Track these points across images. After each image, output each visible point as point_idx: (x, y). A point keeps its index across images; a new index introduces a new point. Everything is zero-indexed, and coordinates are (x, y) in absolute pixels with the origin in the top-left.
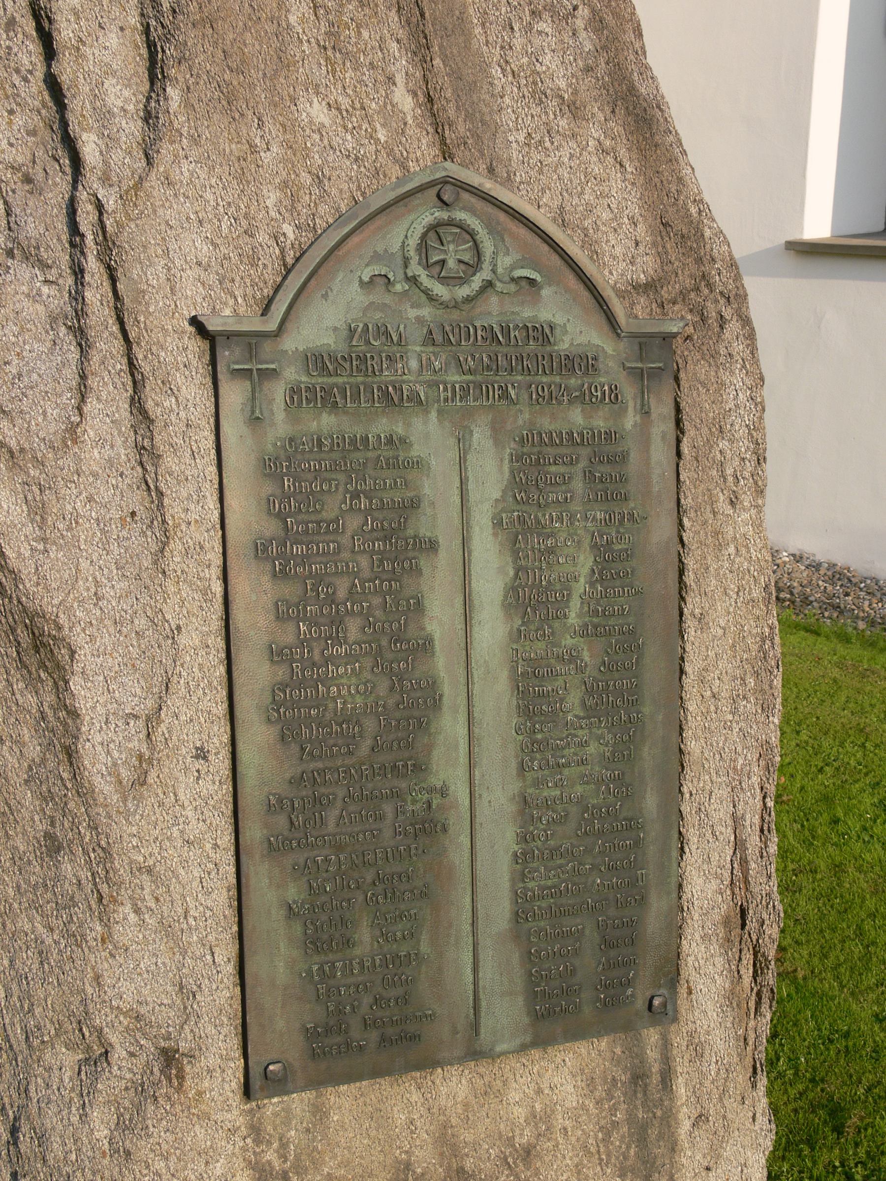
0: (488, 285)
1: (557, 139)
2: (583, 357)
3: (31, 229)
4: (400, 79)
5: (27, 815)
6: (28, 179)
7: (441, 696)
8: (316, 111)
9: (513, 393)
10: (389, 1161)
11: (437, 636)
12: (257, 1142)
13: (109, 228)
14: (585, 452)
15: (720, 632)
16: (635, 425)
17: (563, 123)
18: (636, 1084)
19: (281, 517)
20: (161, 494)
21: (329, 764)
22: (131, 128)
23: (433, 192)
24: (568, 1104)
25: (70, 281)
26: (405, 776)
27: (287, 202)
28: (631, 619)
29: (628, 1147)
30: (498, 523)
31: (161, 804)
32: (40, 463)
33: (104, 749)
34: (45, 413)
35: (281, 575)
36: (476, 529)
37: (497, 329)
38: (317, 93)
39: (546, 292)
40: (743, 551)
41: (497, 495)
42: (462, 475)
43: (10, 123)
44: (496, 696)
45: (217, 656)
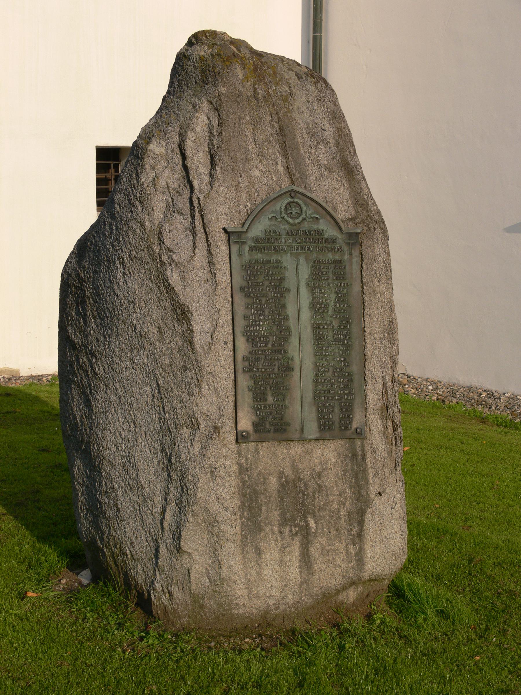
0: (304, 219)
1: (324, 178)
2: (332, 239)
3: (180, 205)
4: (279, 163)
5: (178, 361)
6: (178, 192)
7: (291, 332)
8: (257, 173)
9: (311, 249)
10: (277, 470)
11: (290, 315)
12: (240, 457)
13: (202, 205)
14: (333, 266)
15: (376, 320)
16: (348, 258)
17: (326, 173)
18: (354, 458)
19: (247, 281)
20: (215, 274)
21: (260, 349)
22: (206, 178)
23: (289, 194)
24: (332, 461)
25: (190, 219)
26: (281, 354)
27: (248, 197)
28: (347, 314)
29: (352, 479)
30: (307, 285)
31: (215, 356)
32: (183, 266)
33: (200, 340)
34: (184, 253)
35: (247, 296)
36: (301, 286)
37: (307, 231)
38: (257, 168)
39: (321, 221)
40: (383, 296)
41: (307, 277)
42: (297, 271)
43: (173, 177)
44: (307, 333)
45: (230, 317)
